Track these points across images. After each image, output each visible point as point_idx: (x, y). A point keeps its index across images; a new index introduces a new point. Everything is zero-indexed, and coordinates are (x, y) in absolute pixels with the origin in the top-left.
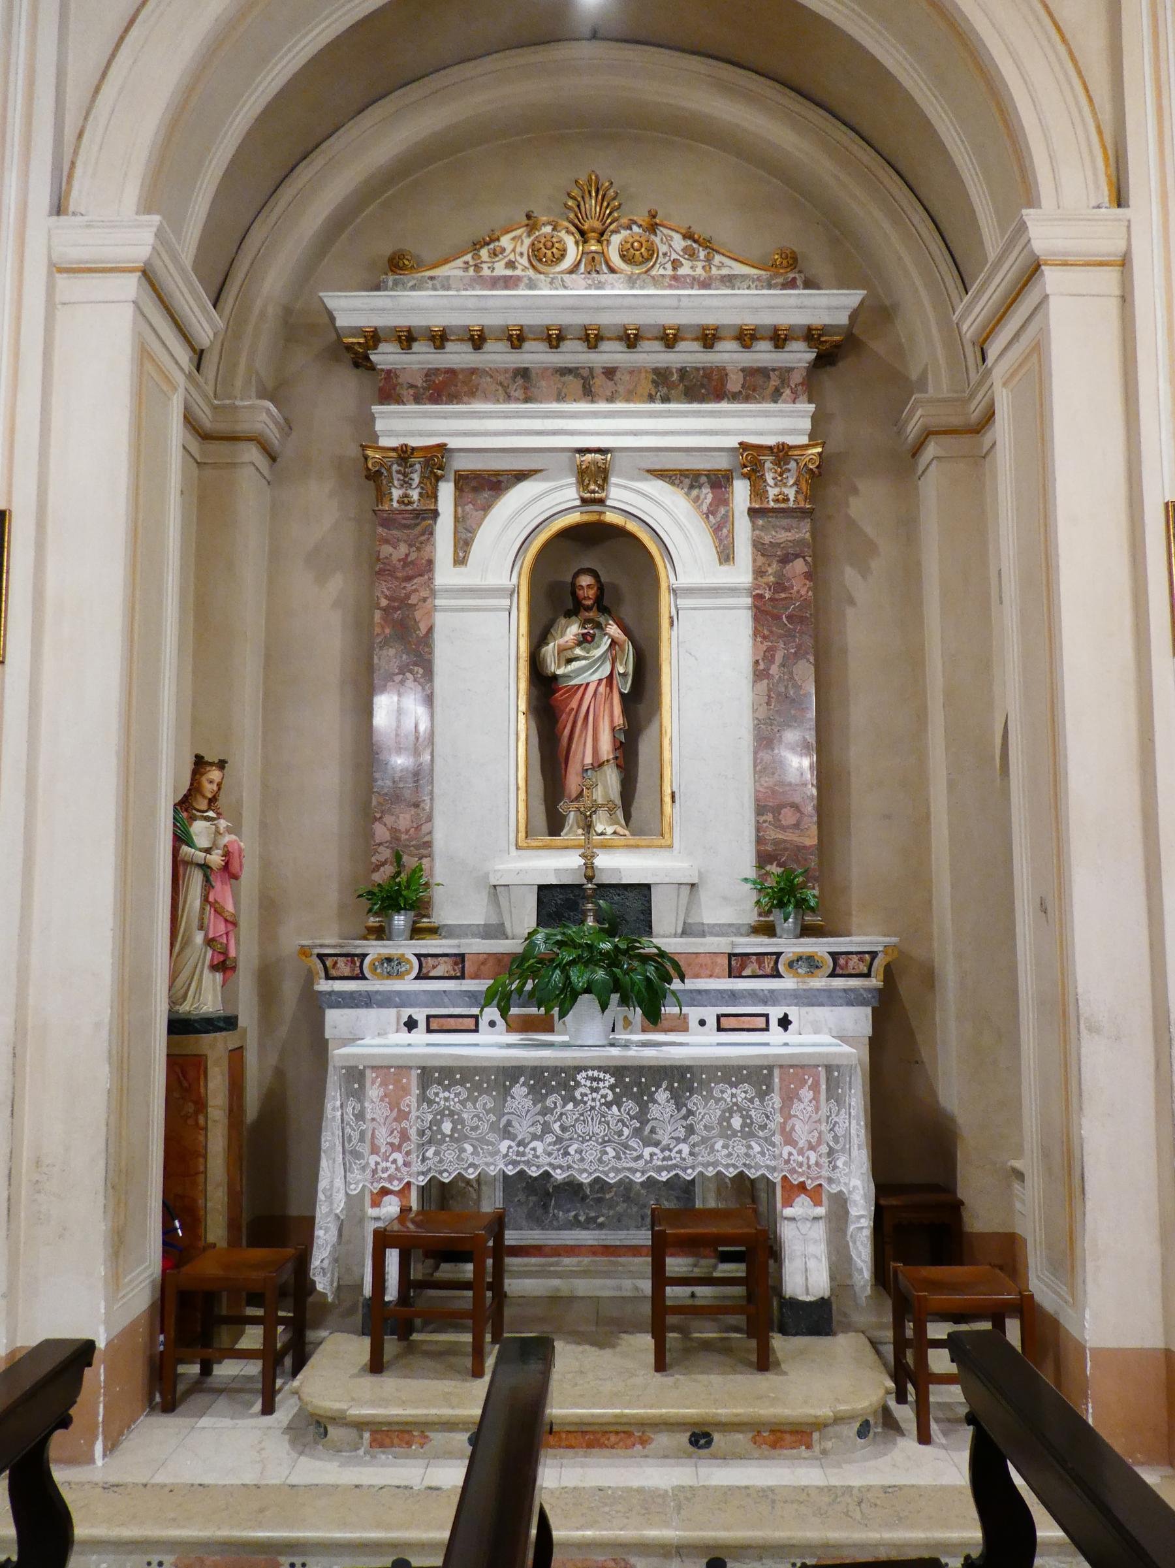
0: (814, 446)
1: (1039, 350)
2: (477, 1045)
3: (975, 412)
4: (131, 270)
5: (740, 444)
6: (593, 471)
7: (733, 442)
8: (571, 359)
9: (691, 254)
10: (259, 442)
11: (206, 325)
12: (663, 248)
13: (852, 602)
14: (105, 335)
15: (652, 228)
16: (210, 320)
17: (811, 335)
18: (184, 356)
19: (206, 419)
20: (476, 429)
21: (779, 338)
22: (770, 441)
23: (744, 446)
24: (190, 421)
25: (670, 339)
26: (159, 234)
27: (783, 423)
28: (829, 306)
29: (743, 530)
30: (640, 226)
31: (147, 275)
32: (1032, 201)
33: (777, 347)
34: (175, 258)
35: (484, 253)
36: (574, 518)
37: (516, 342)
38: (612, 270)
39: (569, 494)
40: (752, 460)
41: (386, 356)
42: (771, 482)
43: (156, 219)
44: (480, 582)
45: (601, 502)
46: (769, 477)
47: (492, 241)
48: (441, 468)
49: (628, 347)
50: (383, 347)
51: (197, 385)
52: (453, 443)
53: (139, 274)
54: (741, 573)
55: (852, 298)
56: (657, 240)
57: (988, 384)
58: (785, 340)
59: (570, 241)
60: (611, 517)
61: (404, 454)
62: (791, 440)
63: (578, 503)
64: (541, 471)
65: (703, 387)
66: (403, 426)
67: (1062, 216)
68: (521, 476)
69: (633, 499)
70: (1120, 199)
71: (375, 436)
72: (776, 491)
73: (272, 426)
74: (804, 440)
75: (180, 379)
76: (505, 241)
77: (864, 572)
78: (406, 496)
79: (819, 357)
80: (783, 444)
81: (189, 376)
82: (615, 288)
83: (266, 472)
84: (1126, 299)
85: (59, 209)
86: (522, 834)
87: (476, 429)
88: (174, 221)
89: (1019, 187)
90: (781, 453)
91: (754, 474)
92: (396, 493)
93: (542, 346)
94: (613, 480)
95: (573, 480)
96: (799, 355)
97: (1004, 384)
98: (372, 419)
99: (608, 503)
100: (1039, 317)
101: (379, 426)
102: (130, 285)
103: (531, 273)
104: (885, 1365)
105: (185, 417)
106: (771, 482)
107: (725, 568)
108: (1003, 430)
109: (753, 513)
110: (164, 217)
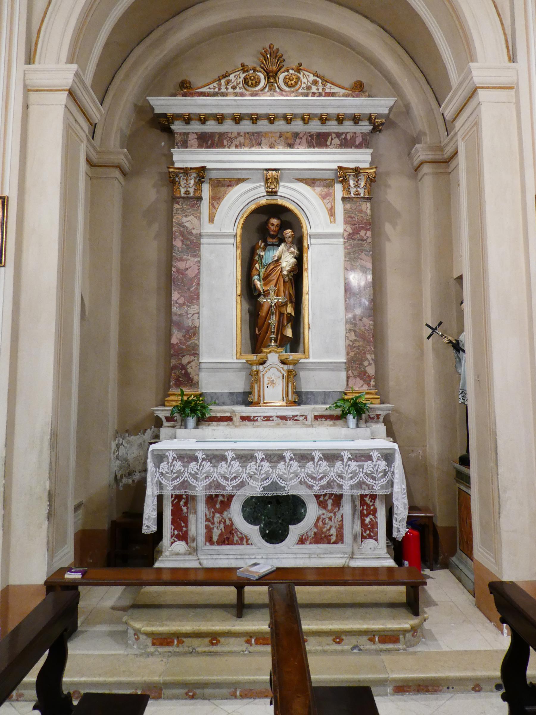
0: (372, 168)
1: (477, 124)
2: (76, 120)
3: (448, 151)
4: (63, 90)
5: (338, 167)
6: (272, 179)
7: (335, 166)
8: (255, 129)
9: (315, 83)
10: (121, 170)
11: (96, 113)
12: (304, 80)
13: (389, 240)
14: (52, 120)
15: (299, 70)
16: (99, 110)
17: (370, 118)
18: (86, 126)
19: (94, 157)
20: (215, 159)
21: (356, 119)
22: (352, 166)
23: (340, 168)
24: (89, 161)
25: (305, 119)
26: (77, 75)
27: (360, 158)
28: (379, 105)
29: (339, 207)
30: (293, 69)
31: (71, 93)
32: (472, 58)
33: (253, 123)
34: (82, 82)
35: (223, 81)
36: (263, 201)
37: (255, 121)
38: (282, 90)
39: (262, 191)
40: (343, 175)
41: (178, 127)
42: (352, 185)
43: (75, 67)
44: (218, 233)
45: (276, 193)
46: (352, 182)
47: (226, 76)
48: (203, 178)
49: (287, 123)
50: (177, 122)
51: (91, 144)
52: (209, 166)
53: (67, 92)
54: (339, 227)
55: (390, 101)
56: (301, 76)
57: (455, 140)
58: (326, 120)
59: (261, 76)
60: (280, 201)
61: (186, 171)
62: (361, 166)
63: (265, 194)
64: (248, 179)
65: (319, 140)
66: (186, 158)
67: (487, 65)
68: (239, 181)
69: (290, 194)
70: (512, 58)
71: (173, 163)
72: (355, 190)
73: (127, 163)
74: (367, 165)
75: (85, 138)
76: (232, 77)
77: (394, 225)
78: (187, 191)
79: (373, 129)
80: (358, 167)
81: (88, 140)
82: (266, 98)
83: (123, 183)
84: (518, 104)
85: (30, 59)
86: (239, 354)
87: (215, 159)
88: (83, 67)
89: (466, 51)
90: (357, 171)
91: (344, 181)
92: (183, 191)
93: (198, 123)
94: (281, 183)
95: (263, 183)
96: (365, 127)
97: (463, 139)
98: (171, 155)
99: (279, 194)
100: (477, 110)
101: (175, 158)
102: (63, 97)
103: (244, 90)
104: (352, 533)
105: (87, 159)
106: (352, 185)
107: (333, 225)
108: (462, 159)
109: (343, 199)
110: (79, 66)
